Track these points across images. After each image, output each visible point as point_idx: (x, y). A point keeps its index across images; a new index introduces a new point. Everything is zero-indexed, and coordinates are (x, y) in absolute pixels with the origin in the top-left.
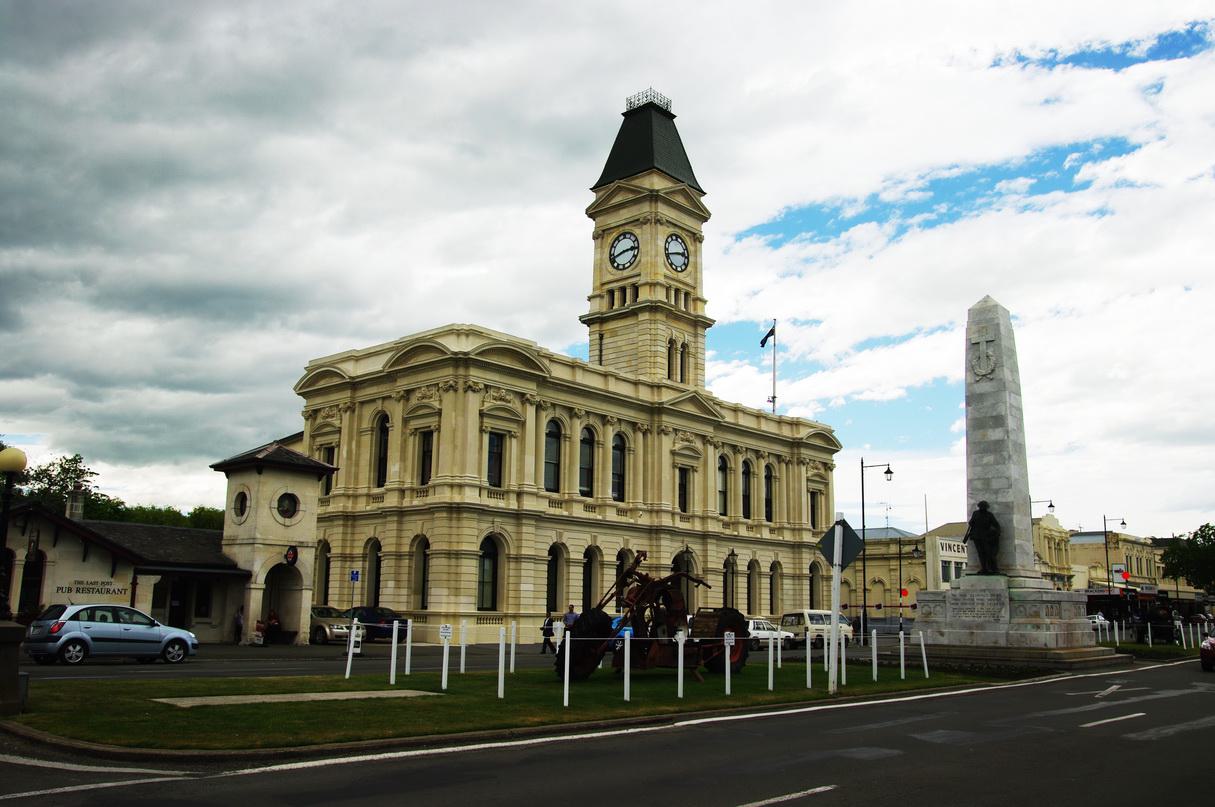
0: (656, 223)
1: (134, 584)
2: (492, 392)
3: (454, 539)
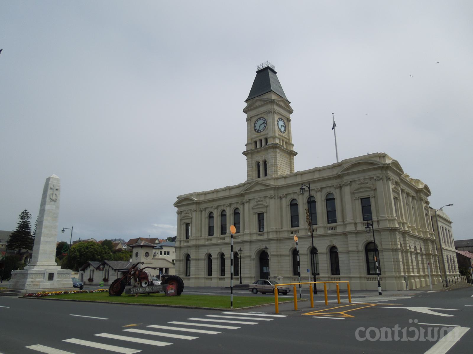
0: (273, 113)
2: (357, 183)
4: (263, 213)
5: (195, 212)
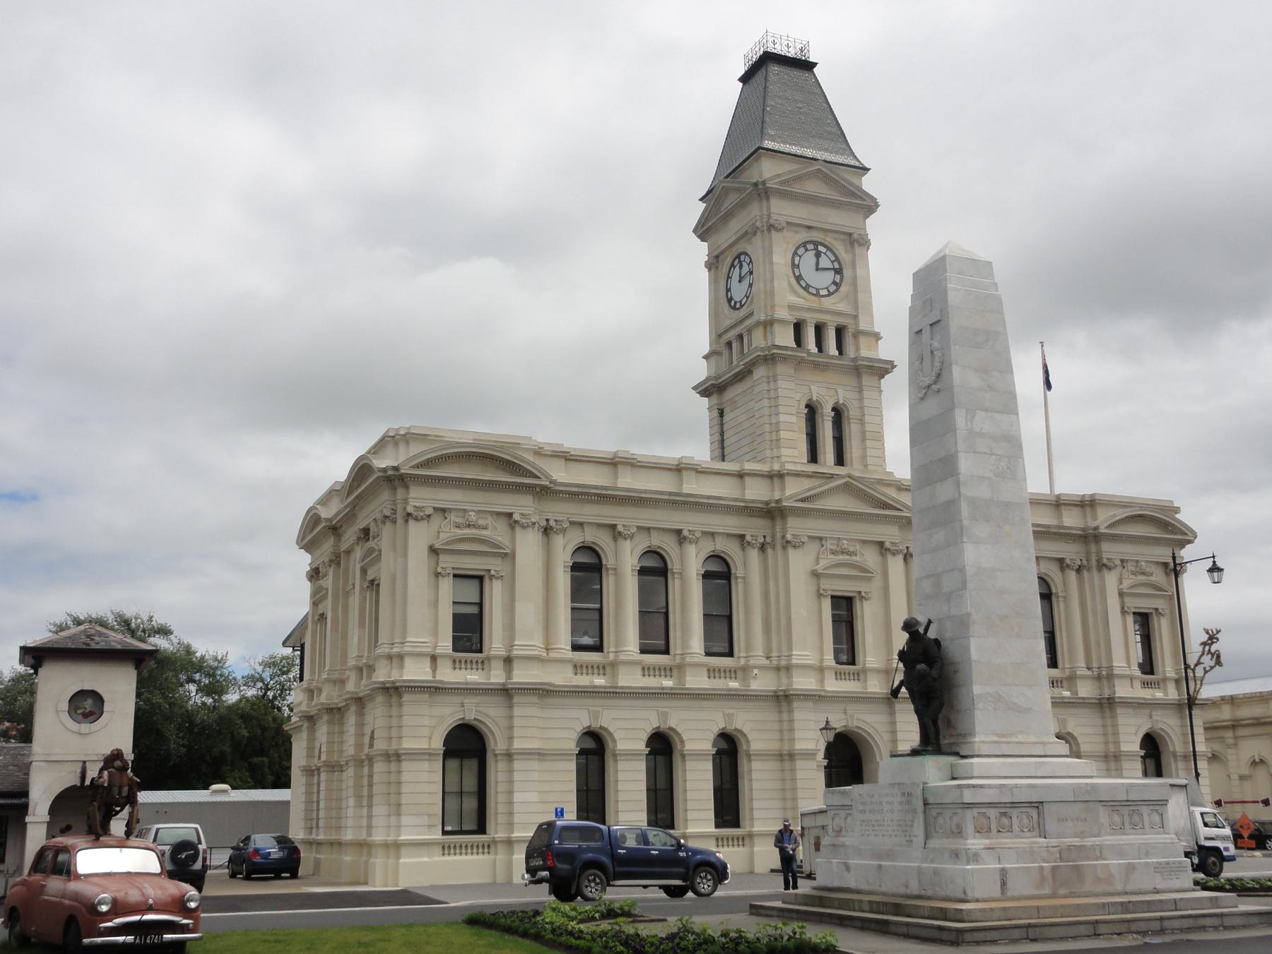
2: (453, 517)
5: (388, 524)
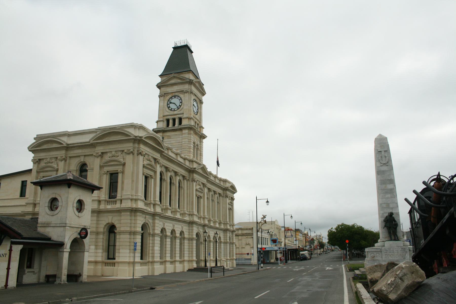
1: (11, 250)
3: (133, 225)
4: (118, 173)
5: (63, 162)
